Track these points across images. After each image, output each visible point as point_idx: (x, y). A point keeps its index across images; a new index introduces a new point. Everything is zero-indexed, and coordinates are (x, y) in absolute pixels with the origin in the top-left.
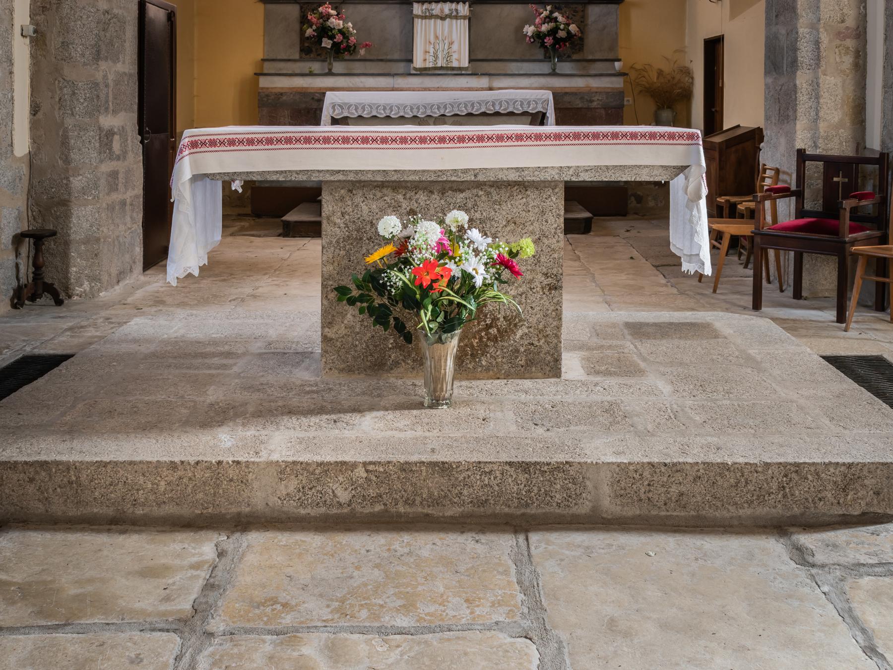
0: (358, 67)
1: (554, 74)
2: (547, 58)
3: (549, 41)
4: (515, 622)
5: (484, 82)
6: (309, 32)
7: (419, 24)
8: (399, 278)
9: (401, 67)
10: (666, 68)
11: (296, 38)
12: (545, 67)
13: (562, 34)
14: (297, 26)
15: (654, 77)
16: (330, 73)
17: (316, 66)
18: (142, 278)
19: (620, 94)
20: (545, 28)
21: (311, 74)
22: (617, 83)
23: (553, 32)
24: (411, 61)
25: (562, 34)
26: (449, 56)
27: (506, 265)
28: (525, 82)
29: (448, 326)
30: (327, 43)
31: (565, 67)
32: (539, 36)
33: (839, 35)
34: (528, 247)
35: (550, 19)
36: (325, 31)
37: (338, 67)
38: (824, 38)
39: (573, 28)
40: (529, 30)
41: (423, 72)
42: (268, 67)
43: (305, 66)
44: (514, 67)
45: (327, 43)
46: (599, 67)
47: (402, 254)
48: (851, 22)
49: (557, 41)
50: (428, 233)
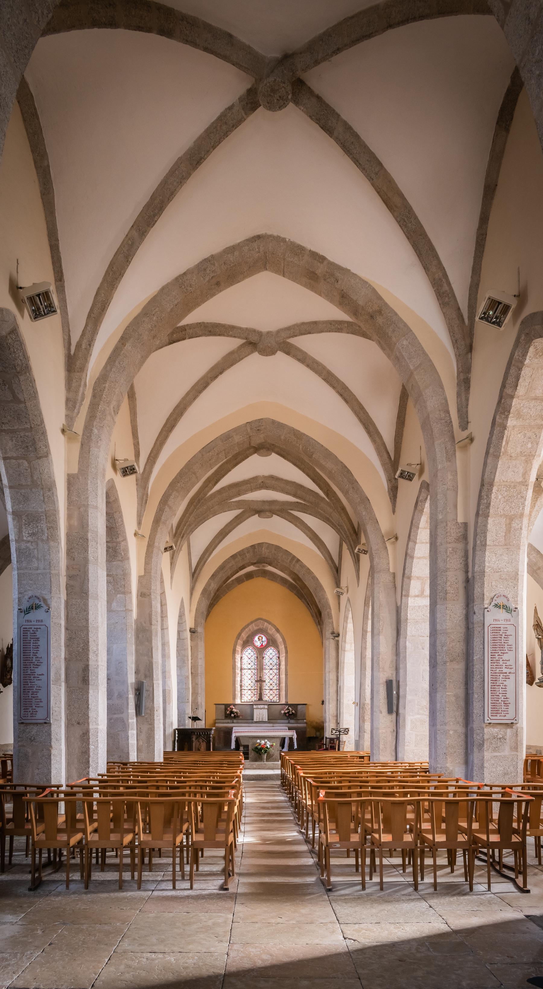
0: (240, 721)
1: (289, 723)
2: (287, 719)
3: (287, 715)
4: (146, 214)
5: (271, 725)
6: (228, 712)
7: (255, 710)
8: (260, 747)
9: (250, 721)
10: (318, 721)
11: (224, 713)
12: (287, 721)
13: (291, 713)
14: (224, 711)
15: (315, 724)
16: (233, 723)
17: (229, 721)
18: (27, 892)
19: (305, 728)
20: (286, 711)
21: (228, 723)
22: (305, 725)
23: (288, 712)
24: (253, 719)
25: (291, 713)
26: (263, 718)
27: (272, 746)
28: (282, 725)
29: (265, 753)
30: (233, 715)
31: (292, 721)
32: (285, 713)
33: (333, 717)
34: (274, 744)
35: (288, 709)
36: (232, 712)
37: (235, 721)
38: (331, 717)
39: (293, 711)
40: (283, 712)
41: (256, 722)
42: (217, 721)
43: (225, 721)
44: (279, 721)
45: (233, 715)
46: (300, 721)
47: (260, 744)
48: (335, 714)
49: (290, 715)
50: (263, 742)
